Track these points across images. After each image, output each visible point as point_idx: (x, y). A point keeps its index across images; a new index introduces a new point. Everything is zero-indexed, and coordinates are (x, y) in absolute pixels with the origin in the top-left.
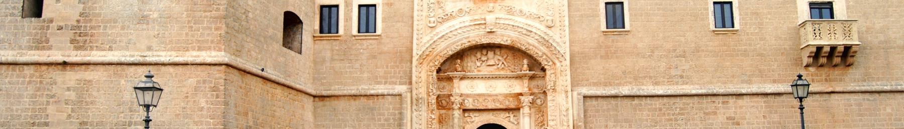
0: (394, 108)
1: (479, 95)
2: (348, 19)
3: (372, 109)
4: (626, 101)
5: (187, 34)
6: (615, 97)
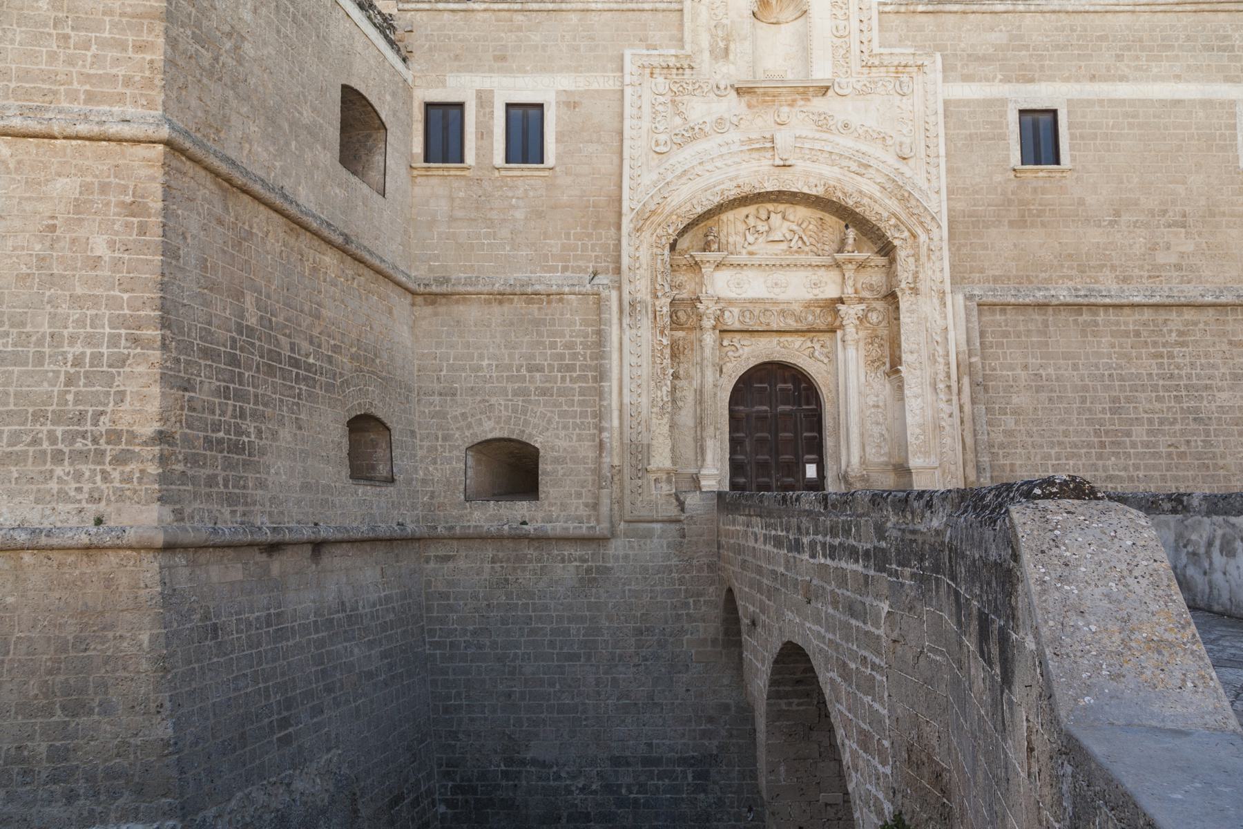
0: (585, 322)
1: (753, 301)
2: (484, 133)
3: (537, 323)
4: (1063, 315)
5: (52, 56)
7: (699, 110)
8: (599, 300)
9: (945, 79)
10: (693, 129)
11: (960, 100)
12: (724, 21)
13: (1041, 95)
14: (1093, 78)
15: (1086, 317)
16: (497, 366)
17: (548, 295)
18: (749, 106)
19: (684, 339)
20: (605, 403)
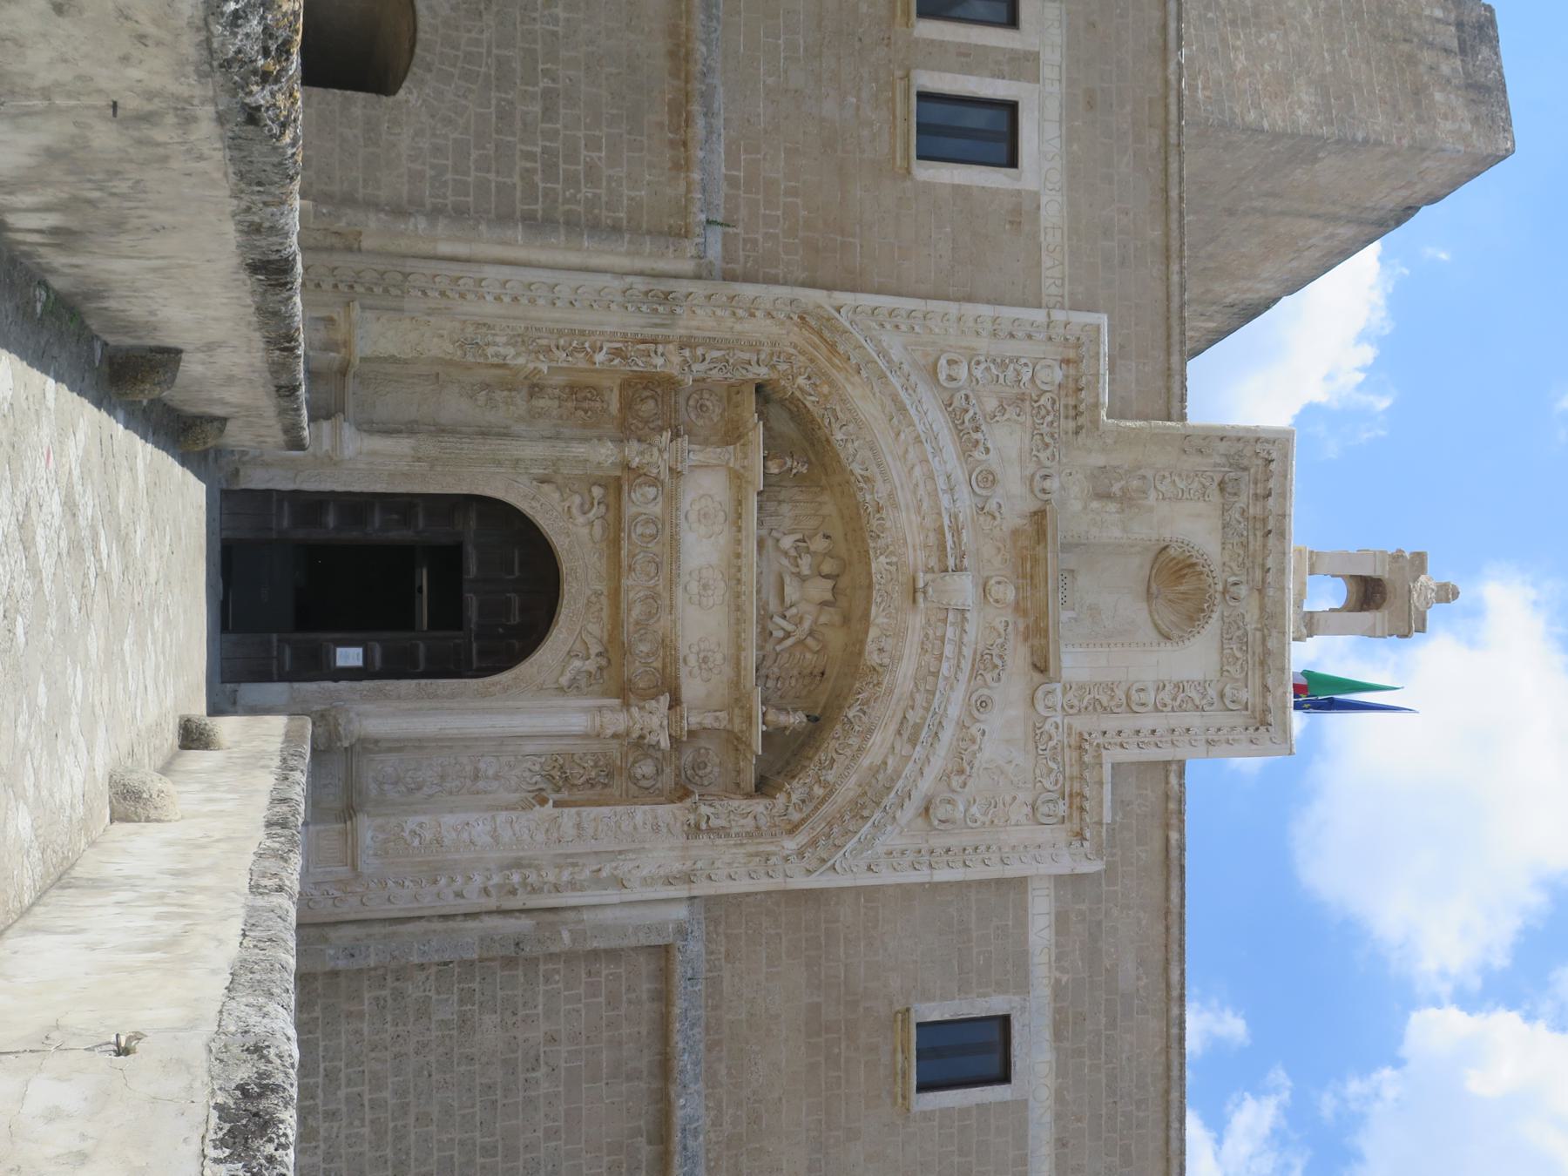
1: (674, 543)
2: (969, 59)
6: (664, 1068)
7: (1007, 442)
8: (678, 235)
9: (1059, 880)
10: (977, 429)
11: (1026, 910)
12: (1152, 495)
13: (1034, 1054)
14: (1061, 1143)
15: (646, 1152)
16: (554, 34)
17: (685, 144)
18: (1015, 533)
19: (605, 410)
20: (483, 227)
